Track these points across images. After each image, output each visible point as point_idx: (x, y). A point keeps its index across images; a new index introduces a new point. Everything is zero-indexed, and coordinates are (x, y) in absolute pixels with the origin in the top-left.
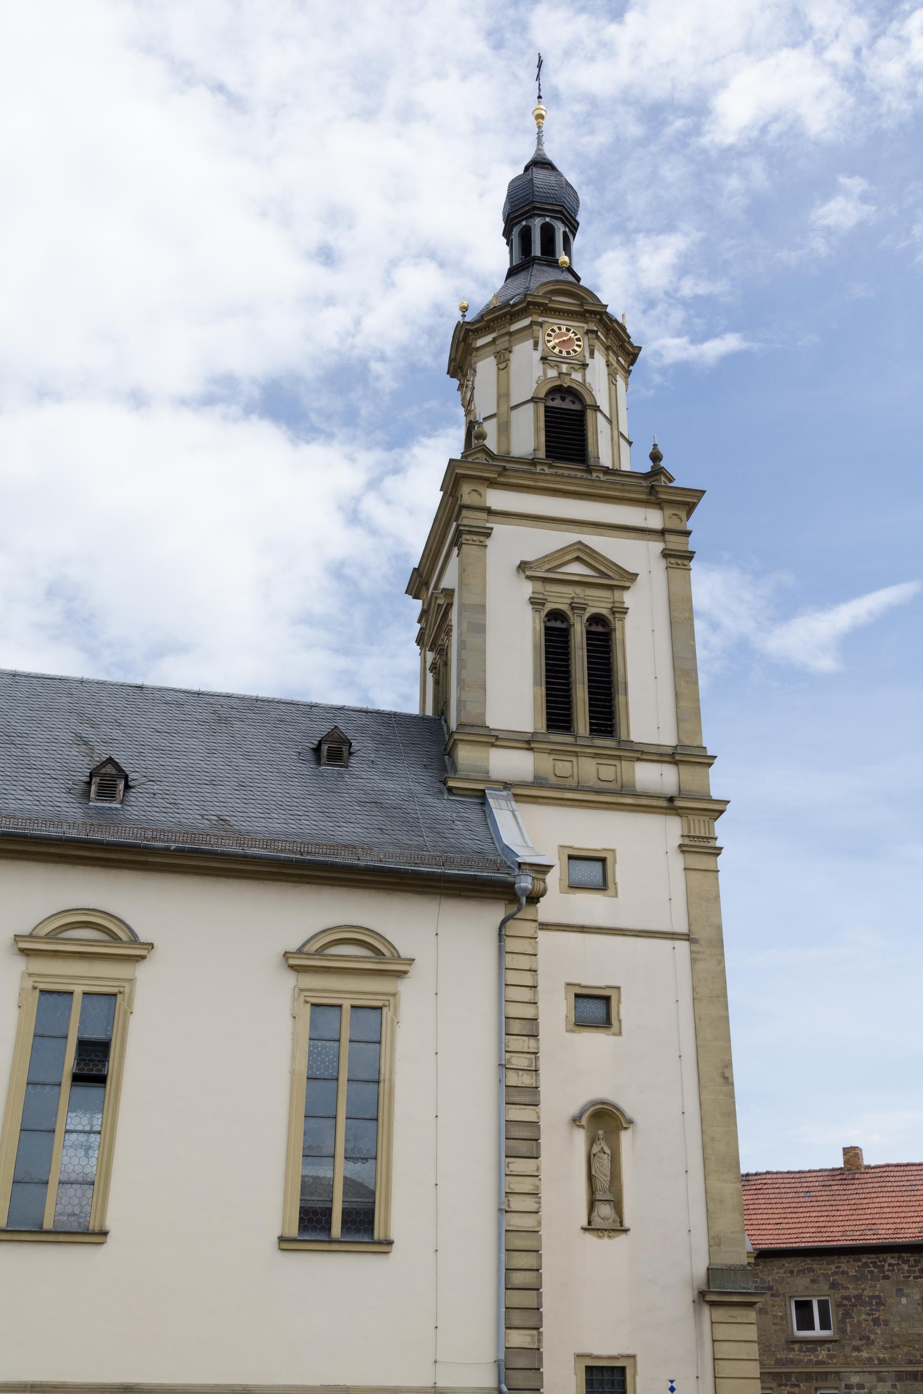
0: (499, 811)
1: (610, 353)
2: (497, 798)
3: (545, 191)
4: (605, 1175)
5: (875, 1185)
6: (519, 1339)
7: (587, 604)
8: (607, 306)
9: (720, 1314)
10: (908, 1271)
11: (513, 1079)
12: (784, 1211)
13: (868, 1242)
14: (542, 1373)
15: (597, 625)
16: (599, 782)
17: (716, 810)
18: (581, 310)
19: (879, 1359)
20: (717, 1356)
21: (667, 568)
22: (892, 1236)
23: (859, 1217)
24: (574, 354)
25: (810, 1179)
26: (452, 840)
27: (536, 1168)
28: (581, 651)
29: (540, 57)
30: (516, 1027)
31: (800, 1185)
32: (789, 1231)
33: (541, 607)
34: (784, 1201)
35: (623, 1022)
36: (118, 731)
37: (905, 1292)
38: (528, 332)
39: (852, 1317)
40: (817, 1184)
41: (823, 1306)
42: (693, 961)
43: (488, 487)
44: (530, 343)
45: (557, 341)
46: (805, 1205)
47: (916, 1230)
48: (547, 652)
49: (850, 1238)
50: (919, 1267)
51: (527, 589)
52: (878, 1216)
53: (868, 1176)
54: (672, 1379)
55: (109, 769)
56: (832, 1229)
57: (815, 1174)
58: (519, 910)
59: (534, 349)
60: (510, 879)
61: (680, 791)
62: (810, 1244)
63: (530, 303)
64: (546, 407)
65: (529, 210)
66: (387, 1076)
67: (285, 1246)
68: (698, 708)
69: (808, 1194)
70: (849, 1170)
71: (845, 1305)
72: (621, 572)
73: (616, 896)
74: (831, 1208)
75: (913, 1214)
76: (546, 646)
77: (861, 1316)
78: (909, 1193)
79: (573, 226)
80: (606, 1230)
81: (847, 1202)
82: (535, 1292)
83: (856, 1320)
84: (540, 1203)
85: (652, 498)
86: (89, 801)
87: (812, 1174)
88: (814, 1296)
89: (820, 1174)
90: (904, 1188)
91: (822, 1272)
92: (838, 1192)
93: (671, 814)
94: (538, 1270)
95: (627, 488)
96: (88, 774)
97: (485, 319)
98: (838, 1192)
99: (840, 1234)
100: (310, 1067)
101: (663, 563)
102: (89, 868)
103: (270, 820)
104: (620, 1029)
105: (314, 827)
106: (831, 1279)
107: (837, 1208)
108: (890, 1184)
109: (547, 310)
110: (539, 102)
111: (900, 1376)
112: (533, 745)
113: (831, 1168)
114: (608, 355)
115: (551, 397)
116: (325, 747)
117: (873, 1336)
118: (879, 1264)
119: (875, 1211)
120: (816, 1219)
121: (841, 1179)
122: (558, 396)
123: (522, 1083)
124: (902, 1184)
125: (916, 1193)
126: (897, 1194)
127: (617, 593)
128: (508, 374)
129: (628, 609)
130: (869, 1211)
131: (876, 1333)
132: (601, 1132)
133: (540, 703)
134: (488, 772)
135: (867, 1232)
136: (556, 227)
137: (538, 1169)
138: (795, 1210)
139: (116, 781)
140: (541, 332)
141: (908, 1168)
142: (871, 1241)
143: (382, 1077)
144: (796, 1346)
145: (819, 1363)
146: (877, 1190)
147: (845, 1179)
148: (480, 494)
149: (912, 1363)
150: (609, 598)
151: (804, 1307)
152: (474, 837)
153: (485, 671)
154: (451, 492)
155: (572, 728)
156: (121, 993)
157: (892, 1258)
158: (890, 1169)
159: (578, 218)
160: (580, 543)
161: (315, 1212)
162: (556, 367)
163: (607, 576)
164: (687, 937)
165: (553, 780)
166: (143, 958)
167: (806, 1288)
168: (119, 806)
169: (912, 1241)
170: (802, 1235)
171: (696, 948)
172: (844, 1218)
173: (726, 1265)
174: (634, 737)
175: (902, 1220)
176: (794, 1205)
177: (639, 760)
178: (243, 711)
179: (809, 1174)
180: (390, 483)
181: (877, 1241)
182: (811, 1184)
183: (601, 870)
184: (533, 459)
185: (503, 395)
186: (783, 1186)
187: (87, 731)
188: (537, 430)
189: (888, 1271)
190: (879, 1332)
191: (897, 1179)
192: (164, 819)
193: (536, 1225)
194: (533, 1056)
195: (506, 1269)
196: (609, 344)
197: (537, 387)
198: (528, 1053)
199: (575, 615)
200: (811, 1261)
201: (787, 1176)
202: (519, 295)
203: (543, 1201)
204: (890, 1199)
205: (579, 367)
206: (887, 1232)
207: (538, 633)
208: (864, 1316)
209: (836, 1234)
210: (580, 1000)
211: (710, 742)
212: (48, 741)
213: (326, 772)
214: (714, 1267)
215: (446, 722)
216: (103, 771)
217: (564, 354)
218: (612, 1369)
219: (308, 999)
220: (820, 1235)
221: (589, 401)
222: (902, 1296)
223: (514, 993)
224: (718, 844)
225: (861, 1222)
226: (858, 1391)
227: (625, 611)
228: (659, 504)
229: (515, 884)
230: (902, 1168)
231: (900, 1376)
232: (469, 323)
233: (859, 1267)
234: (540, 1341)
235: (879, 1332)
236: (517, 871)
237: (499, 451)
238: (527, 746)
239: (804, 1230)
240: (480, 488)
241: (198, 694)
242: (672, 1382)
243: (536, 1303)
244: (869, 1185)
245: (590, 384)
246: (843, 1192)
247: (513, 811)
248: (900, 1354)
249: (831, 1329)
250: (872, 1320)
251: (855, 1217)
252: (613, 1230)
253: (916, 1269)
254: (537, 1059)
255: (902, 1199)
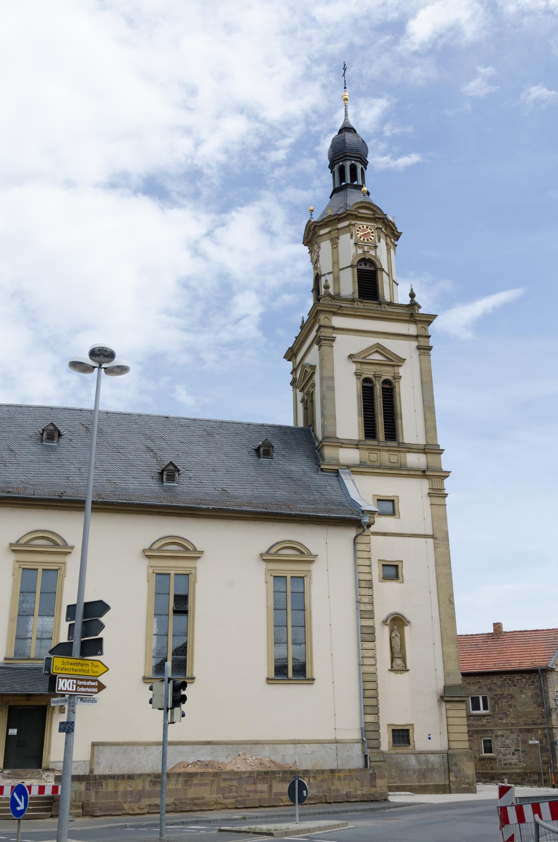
0: (347, 481)
1: (388, 238)
2: (344, 473)
3: (351, 146)
4: (398, 646)
5: (509, 641)
6: (370, 718)
7: (382, 375)
8: (387, 215)
9: (450, 706)
10: (526, 682)
11: (363, 607)
12: (465, 654)
13: (506, 669)
14: (380, 732)
15: (386, 384)
16: (390, 463)
17: (445, 475)
18: (374, 217)
19: (511, 723)
20: (449, 724)
21: (419, 355)
22: (518, 666)
23: (502, 657)
24: (371, 241)
25: (477, 639)
26: (327, 497)
27: (374, 646)
28: (380, 398)
29: (345, 65)
30: (363, 584)
31: (472, 641)
32: (468, 664)
33: (360, 377)
34: (465, 649)
35: (404, 577)
36: (164, 443)
37: (524, 692)
38: (348, 229)
39: (498, 704)
40: (480, 641)
41: (485, 699)
42: (435, 548)
43: (332, 315)
44: (348, 235)
45: (362, 234)
46: (475, 651)
47: (530, 663)
48: (364, 399)
49: (498, 667)
50: (531, 680)
51: (353, 367)
52: (511, 656)
53: (506, 637)
54: (429, 734)
55: (171, 467)
56: (489, 663)
57: (479, 636)
58: (363, 531)
59: (351, 239)
60: (359, 518)
61: (428, 467)
62: (478, 670)
63: (348, 214)
64: (358, 269)
65: (344, 156)
66: (308, 607)
67: (269, 682)
68: (435, 426)
69: (476, 646)
70: (496, 634)
71: (495, 698)
72: (398, 358)
73: (399, 518)
74: (488, 653)
75: (528, 655)
76: (363, 396)
77: (503, 703)
78: (526, 645)
79: (365, 163)
80: (399, 670)
81: (496, 650)
82: (376, 699)
83: (500, 705)
84: (376, 661)
85: (412, 319)
86: (163, 483)
87: (478, 636)
88: (480, 695)
89: (482, 636)
90: (523, 643)
91: (484, 683)
92: (491, 645)
93: (424, 478)
94: (376, 690)
95: (400, 314)
96: (162, 470)
97: (325, 221)
98: (491, 645)
99: (493, 665)
100: (274, 604)
101: (417, 352)
102: (172, 517)
103: (245, 489)
104: (403, 580)
105: (265, 492)
106: (489, 686)
107: (491, 653)
108: (516, 641)
109: (357, 217)
110: (345, 91)
111: (521, 731)
112: (359, 447)
113: (487, 633)
114: (386, 239)
115: (359, 264)
116: (262, 449)
117: (509, 713)
118: (511, 679)
119: (510, 654)
120: (481, 658)
121: (492, 639)
122: (363, 263)
123: (367, 609)
124: (522, 640)
125: (529, 645)
126: (520, 645)
127: (396, 368)
128: (338, 251)
129: (401, 376)
130: (506, 654)
131: (510, 711)
132: (395, 627)
133: (361, 424)
134: (339, 460)
135: (506, 664)
136: (357, 166)
137: (375, 646)
138: (470, 654)
139: (174, 473)
140: (354, 229)
141: (525, 633)
142: (508, 669)
143: (306, 608)
144: (472, 718)
145: (482, 725)
146: (510, 643)
147: (494, 639)
148: (329, 319)
149: (527, 725)
150: (392, 371)
151: (475, 701)
152: (337, 494)
153: (335, 410)
154: (314, 317)
155: (376, 437)
156: (191, 573)
157: (518, 676)
158: (516, 633)
159: (368, 159)
160: (378, 344)
161: (281, 667)
162: (362, 248)
163: (392, 360)
164: (432, 537)
165: (369, 463)
166: (199, 557)
167: (476, 691)
168: (177, 485)
169: (528, 668)
170: (474, 666)
171: (437, 541)
172: (494, 658)
173: (452, 685)
174: (406, 441)
175: (523, 658)
176: (469, 651)
177: (409, 452)
178: (218, 429)
179: (476, 636)
180: (219, 232)
181: (511, 668)
182: (477, 641)
183: (392, 506)
184: (353, 299)
185: (335, 262)
186: (464, 642)
187: (151, 444)
188: (354, 282)
189: (516, 682)
190: (512, 711)
191: (520, 638)
192: (199, 491)
193: (375, 670)
194: (371, 597)
195: (363, 690)
196: (387, 233)
197: (353, 259)
198: (369, 595)
199: (377, 380)
200: (479, 678)
201: (465, 637)
202: (342, 208)
203: (377, 660)
204: (517, 648)
205: (373, 247)
206: (516, 664)
207: (359, 390)
208: (504, 704)
209: (491, 665)
210: (384, 567)
211: (442, 442)
212: (135, 450)
213: (263, 462)
214: (447, 685)
215: (313, 431)
216: (168, 468)
217: (366, 241)
218: (403, 730)
219: (272, 574)
220: (483, 666)
221: (379, 267)
222: (523, 694)
223: (361, 569)
224: (446, 492)
225: (503, 659)
226: (501, 738)
227: (400, 378)
228: (415, 322)
229: (361, 520)
230: (522, 633)
231: (521, 731)
232: (316, 222)
233: (502, 680)
234: (378, 719)
235: (512, 711)
236: (361, 515)
237: (334, 293)
238: (356, 447)
239: (475, 664)
240: (328, 316)
241: (195, 420)
242: (429, 735)
243: (376, 703)
244: (506, 641)
245: (379, 257)
246: (494, 645)
247: (353, 481)
248: (521, 721)
249: (488, 710)
250: (508, 705)
251: (500, 657)
252: (402, 670)
253: (529, 681)
254: (373, 598)
255: (522, 648)
